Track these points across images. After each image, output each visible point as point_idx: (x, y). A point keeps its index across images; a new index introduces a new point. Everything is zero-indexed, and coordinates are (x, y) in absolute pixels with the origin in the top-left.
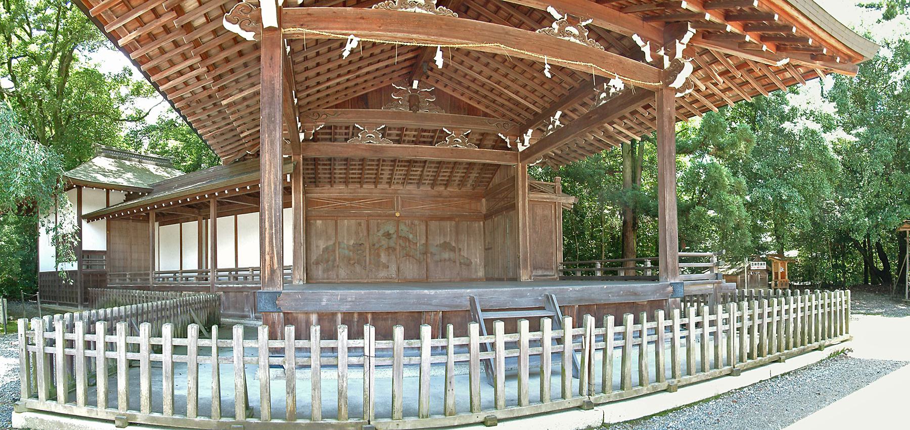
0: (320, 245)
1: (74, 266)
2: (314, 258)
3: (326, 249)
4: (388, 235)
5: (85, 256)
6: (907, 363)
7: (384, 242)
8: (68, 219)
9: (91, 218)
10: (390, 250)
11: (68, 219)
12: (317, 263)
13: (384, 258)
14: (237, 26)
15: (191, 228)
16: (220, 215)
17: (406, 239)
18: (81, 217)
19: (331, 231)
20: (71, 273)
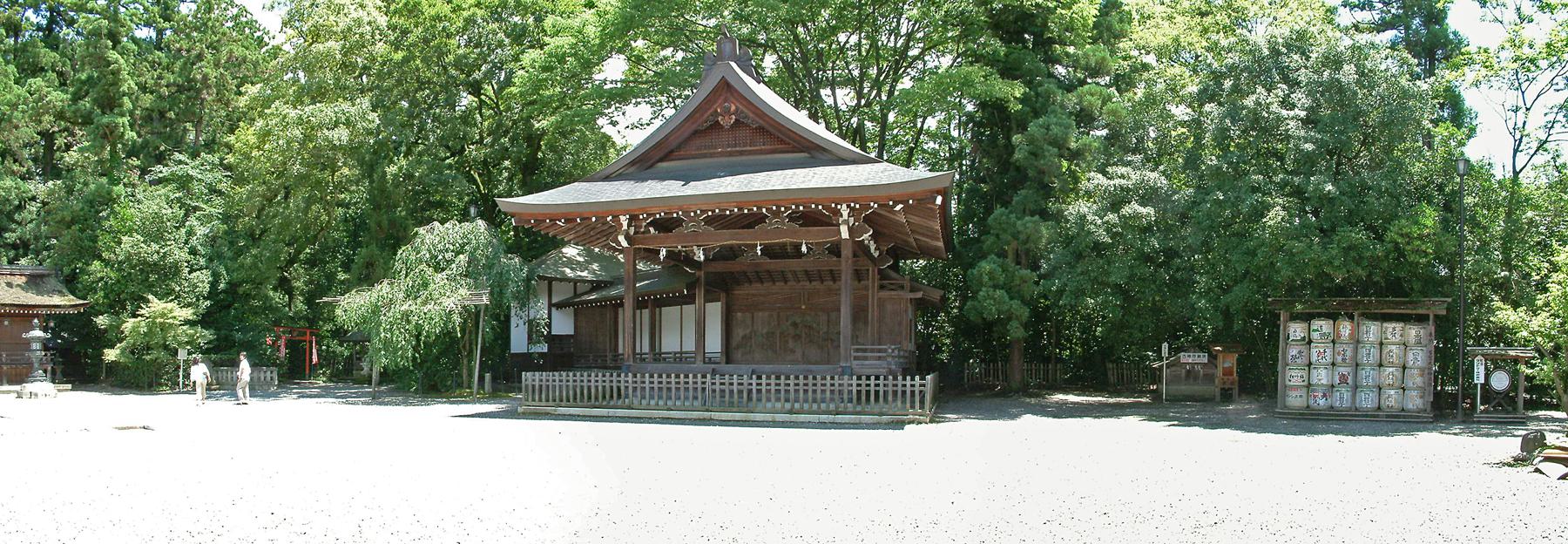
0: (739, 333)
1: (544, 348)
2: (734, 343)
3: (744, 337)
4: (795, 325)
5: (552, 339)
6: (1022, 37)
7: (792, 331)
8: (540, 309)
9: (559, 306)
10: (797, 337)
11: (540, 309)
12: (738, 347)
13: (791, 344)
14: (805, 112)
15: (689, 310)
16: (707, 301)
17: (810, 328)
18: (550, 305)
19: (749, 322)
20: (542, 355)
